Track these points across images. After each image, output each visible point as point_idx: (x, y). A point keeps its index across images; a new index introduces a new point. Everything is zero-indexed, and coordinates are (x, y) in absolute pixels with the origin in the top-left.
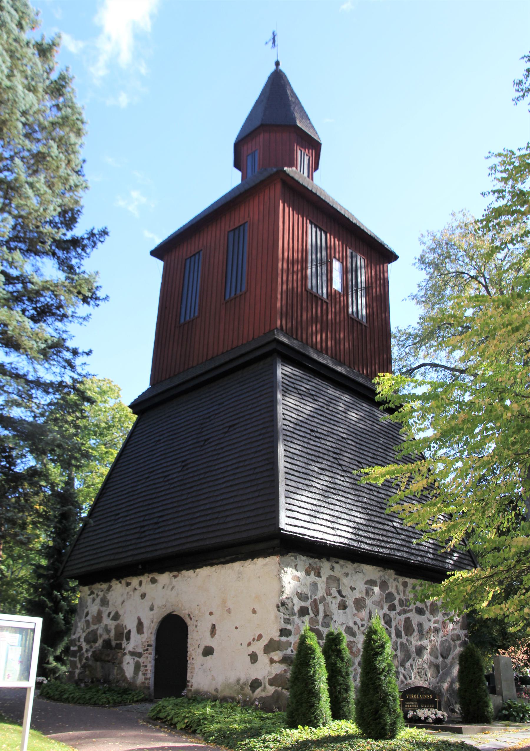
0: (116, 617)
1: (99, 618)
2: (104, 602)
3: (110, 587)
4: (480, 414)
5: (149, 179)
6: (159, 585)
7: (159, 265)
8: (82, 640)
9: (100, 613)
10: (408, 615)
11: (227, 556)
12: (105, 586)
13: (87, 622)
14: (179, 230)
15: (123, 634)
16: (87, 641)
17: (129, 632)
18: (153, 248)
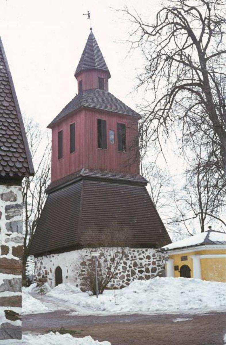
0: (45, 268)
1: (40, 269)
2: (41, 263)
3: (42, 258)
4: (224, 123)
5: (43, 96)
6: (54, 258)
7: (50, 130)
8: (37, 275)
9: (41, 266)
10: (135, 261)
11: (36, 231)
12: (41, 258)
13: (38, 270)
14: (78, 90)
15: (47, 273)
16: (38, 276)
17: (48, 272)
18: (47, 125)
